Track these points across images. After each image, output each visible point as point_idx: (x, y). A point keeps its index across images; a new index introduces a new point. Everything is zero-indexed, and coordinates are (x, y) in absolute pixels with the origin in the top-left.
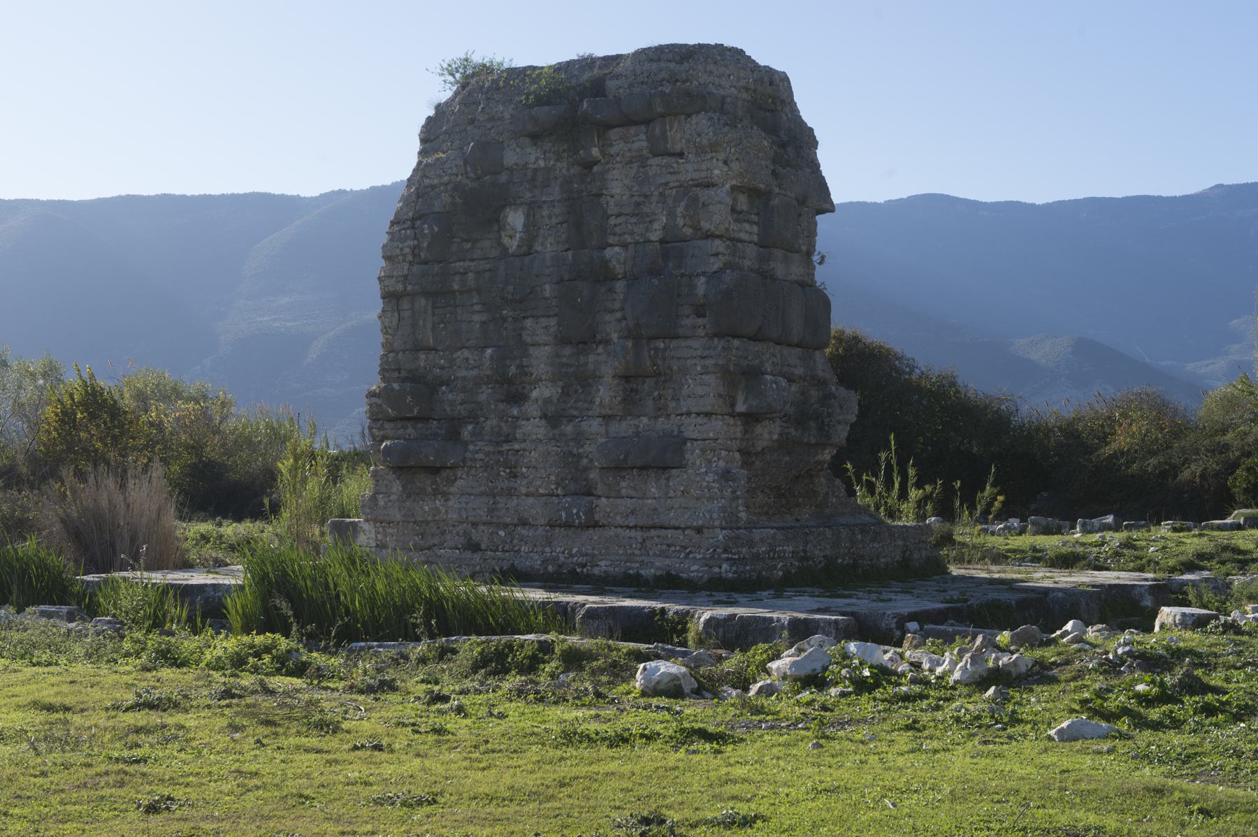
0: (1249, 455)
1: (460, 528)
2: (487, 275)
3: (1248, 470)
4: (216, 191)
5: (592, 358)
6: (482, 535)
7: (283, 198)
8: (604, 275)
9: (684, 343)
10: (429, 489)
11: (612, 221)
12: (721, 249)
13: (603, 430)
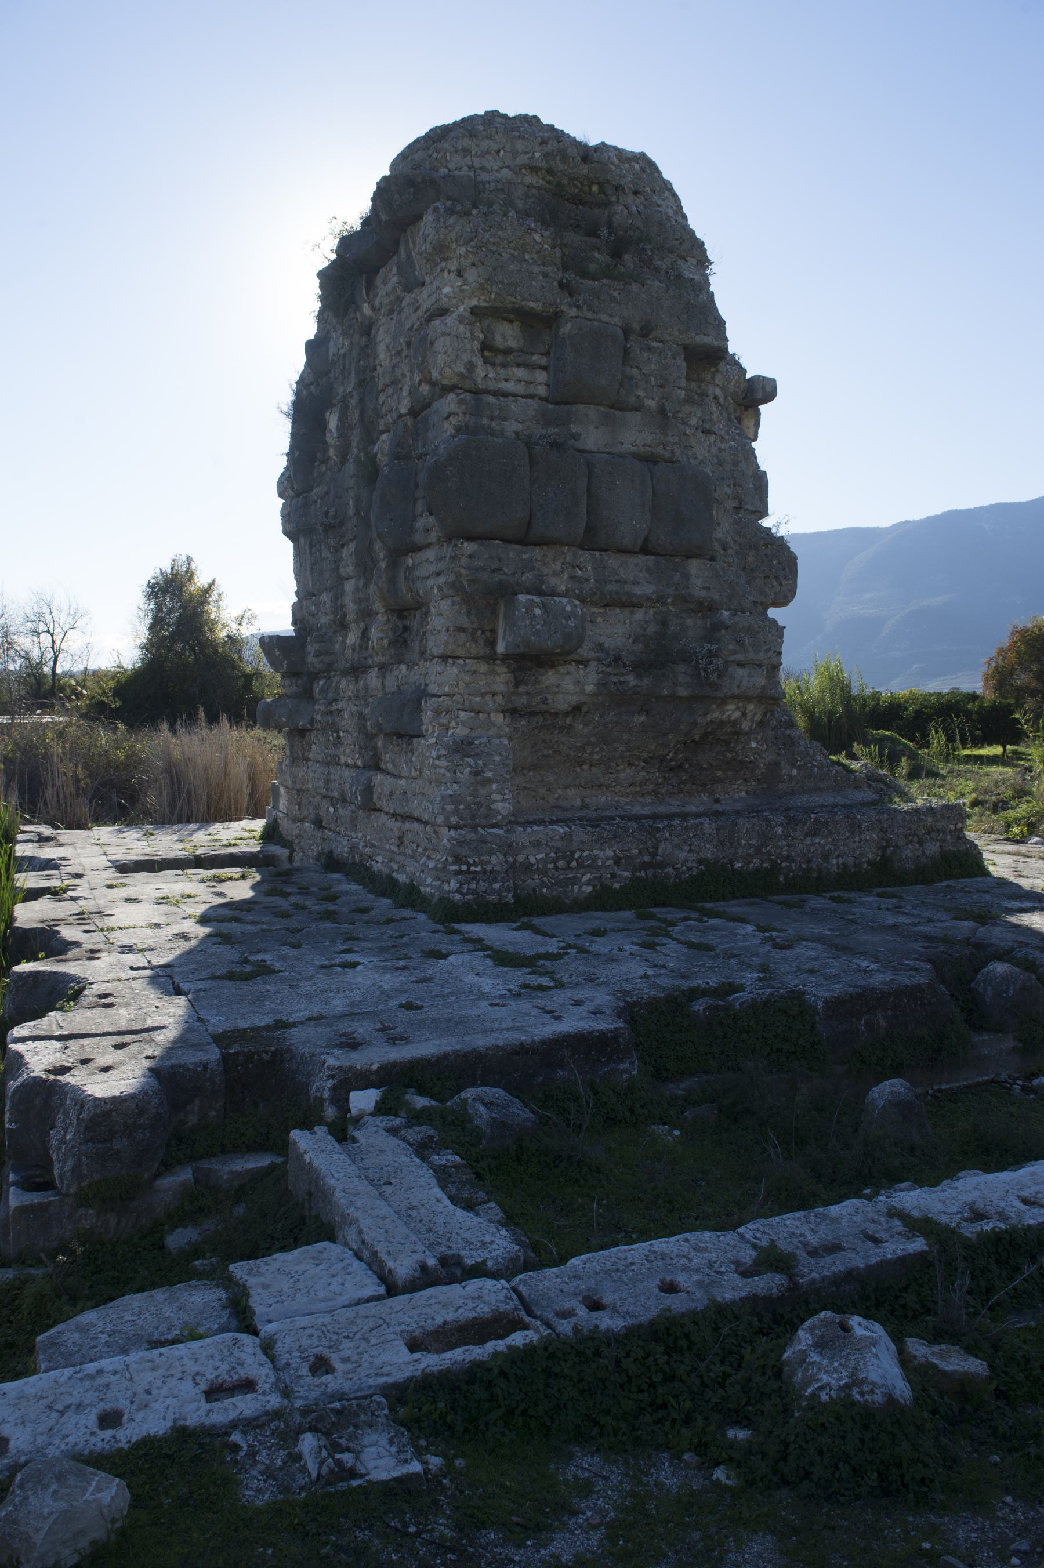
7: (868, 529)
12: (453, 407)
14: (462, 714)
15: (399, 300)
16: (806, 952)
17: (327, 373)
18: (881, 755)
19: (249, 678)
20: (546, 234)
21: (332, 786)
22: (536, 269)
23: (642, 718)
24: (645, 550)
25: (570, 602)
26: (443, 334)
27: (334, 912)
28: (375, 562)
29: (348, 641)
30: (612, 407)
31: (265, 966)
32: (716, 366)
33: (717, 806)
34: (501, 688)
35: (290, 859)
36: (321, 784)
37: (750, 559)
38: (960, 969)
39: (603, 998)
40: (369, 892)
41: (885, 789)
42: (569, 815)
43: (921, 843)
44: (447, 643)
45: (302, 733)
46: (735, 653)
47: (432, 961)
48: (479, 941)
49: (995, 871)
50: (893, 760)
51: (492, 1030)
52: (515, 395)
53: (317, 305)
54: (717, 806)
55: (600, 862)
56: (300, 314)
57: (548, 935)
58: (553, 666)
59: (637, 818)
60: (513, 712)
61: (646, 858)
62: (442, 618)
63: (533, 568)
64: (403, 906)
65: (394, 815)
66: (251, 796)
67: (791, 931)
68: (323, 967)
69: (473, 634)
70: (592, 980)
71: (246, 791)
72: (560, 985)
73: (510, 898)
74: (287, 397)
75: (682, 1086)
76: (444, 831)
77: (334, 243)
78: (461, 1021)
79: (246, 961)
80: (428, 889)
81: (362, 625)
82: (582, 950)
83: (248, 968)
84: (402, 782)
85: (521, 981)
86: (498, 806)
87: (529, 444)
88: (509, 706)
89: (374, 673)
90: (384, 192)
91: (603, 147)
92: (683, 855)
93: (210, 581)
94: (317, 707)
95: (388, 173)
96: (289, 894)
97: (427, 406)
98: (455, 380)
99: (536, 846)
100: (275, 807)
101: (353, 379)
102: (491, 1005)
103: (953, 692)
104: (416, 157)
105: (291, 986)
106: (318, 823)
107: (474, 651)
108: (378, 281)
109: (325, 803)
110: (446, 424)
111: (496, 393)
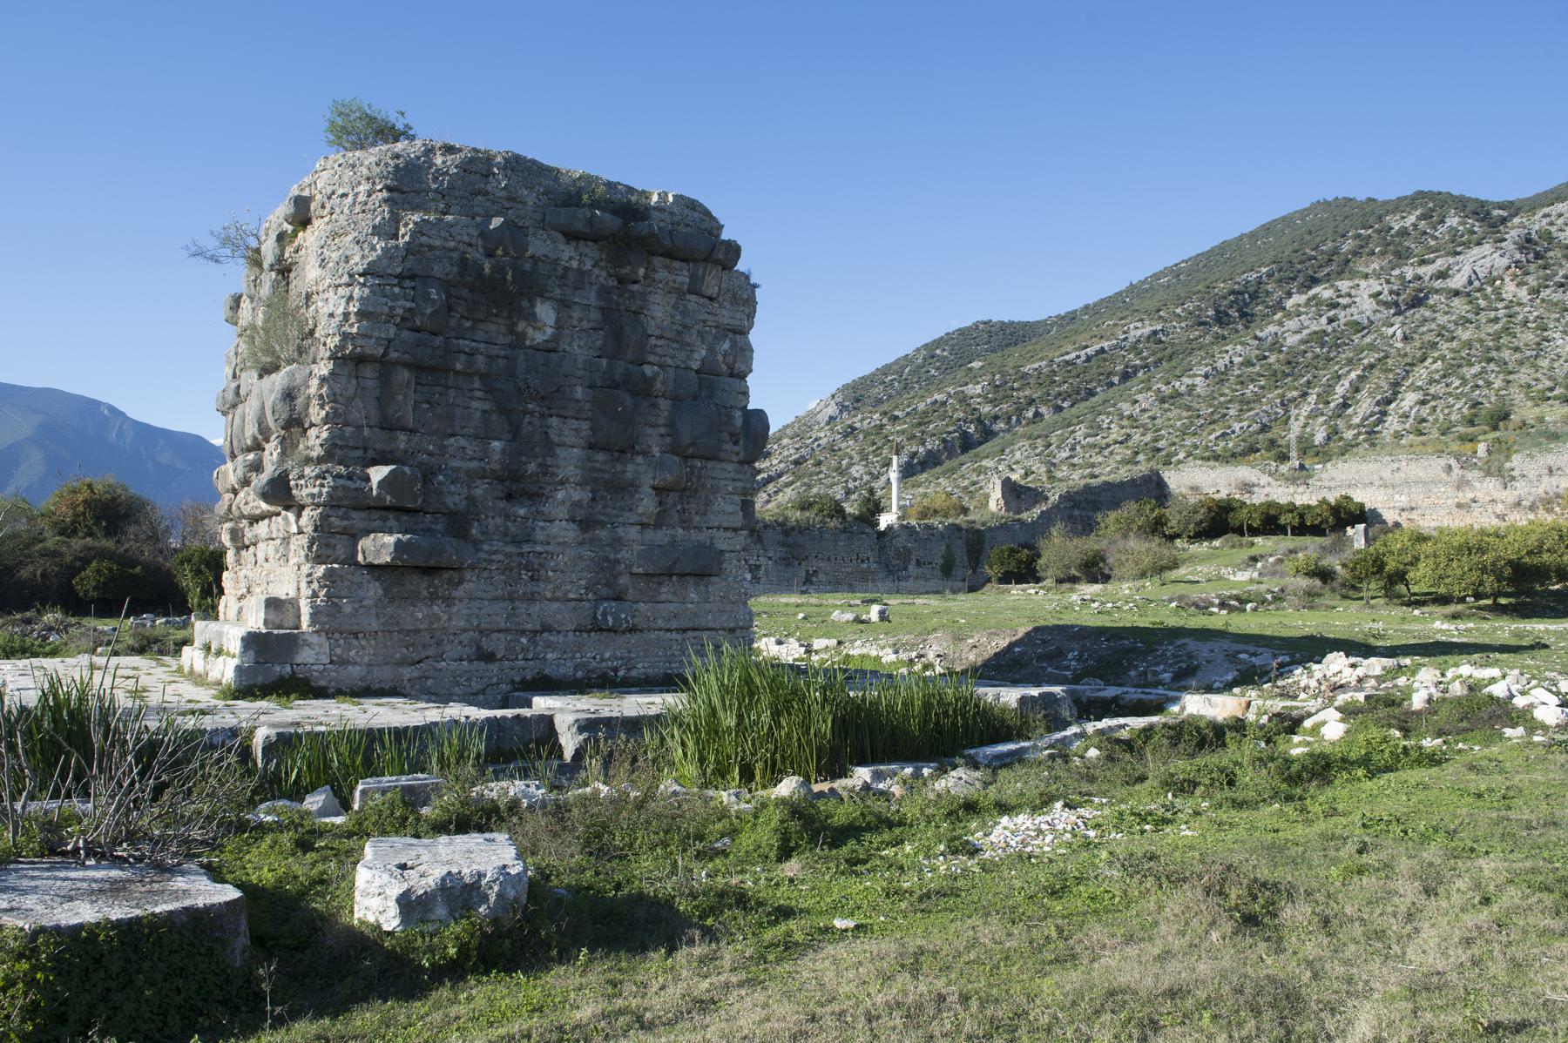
1: (465, 637)
2: (502, 362)
5: (630, 467)
6: (497, 644)
8: (642, 390)
9: (719, 465)
10: (425, 593)
11: (653, 341)
13: (639, 537)
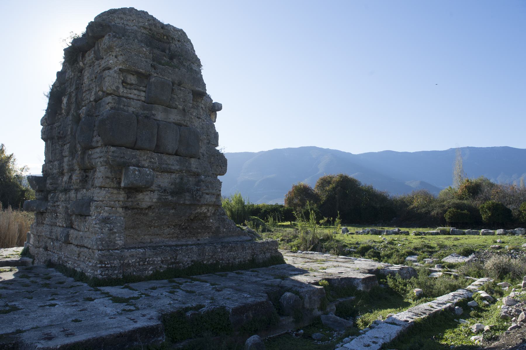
0: (450, 208)
3: (450, 212)
4: (238, 152)
12: (110, 101)
14: (106, 208)
15: (93, 62)
16: (227, 292)
17: (64, 84)
18: (254, 225)
19: (23, 192)
20: (148, 49)
21: (53, 234)
22: (143, 59)
23: (173, 211)
24: (176, 154)
25: (149, 170)
26: (108, 76)
27: (49, 284)
28: (76, 151)
29: (64, 180)
30: (167, 107)
31: (15, 307)
32: (202, 98)
33: (199, 242)
34: (122, 199)
35: (33, 263)
36: (48, 233)
37: (212, 159)
38: (275, 295)
39: (153, 313)
40: (65, 275)
41: (253, 235)
42: (145, 245)
43: (265, 253)
44: (102, 182)
45: (42, 213)
46: (206, 190)
47: (87, 302)
48: (108, 293)
49: (287, 262)
50: (257, 226)
51: (109, 328)
52: (133, 99)
53: (63, 60)
54: (199, 242)
55: (156, 262)
56: (56, 63)
57: (134, 290)
58: (142, 192)
59: (170, 246)
60: (126, 208)
61: (173, 261)
62: (101, 173)
63: (136, 158)
64: (78, 281)
65: (77, 246)
66: (19, 237)
67: (222, 285)
68: (41, 306)
69: (112, 179)
70: (150, 307)
71: (17, 236)
72: (138, 309)
73: (121, 276)
74: (48, 90)
75: (182, 344)
76: (96, 251)
77: (71, 40)
78: (97, 326)
79: (7, 305)
80: (89, 274)
81: (70, 174)
82: (147, 295)
83: (7, 308)
84: (81, 233)
85: (123, 308)
86: (119, 242)
87: (137, 115)
88: (125, 205)
89: (73, 192)
90: (91, 26)
91: (168, 25)
92: (186, 259)
93: (11, 154)
94: (49, 204)
95: (93, 21)
96: (30, 277)
97: (101, 99)
98: (112, 92)
99: (132, 257)
100: (28, 242)
101: (74, 87)
102: (110, 318)
103: (277, 205)
104: (104, 17)
105: (26, 315)
106: (46, 249)
107: (112, 185)
108: (87, 55)
109: (49, 241)
110: (107, 106)
111: (126, 98)
